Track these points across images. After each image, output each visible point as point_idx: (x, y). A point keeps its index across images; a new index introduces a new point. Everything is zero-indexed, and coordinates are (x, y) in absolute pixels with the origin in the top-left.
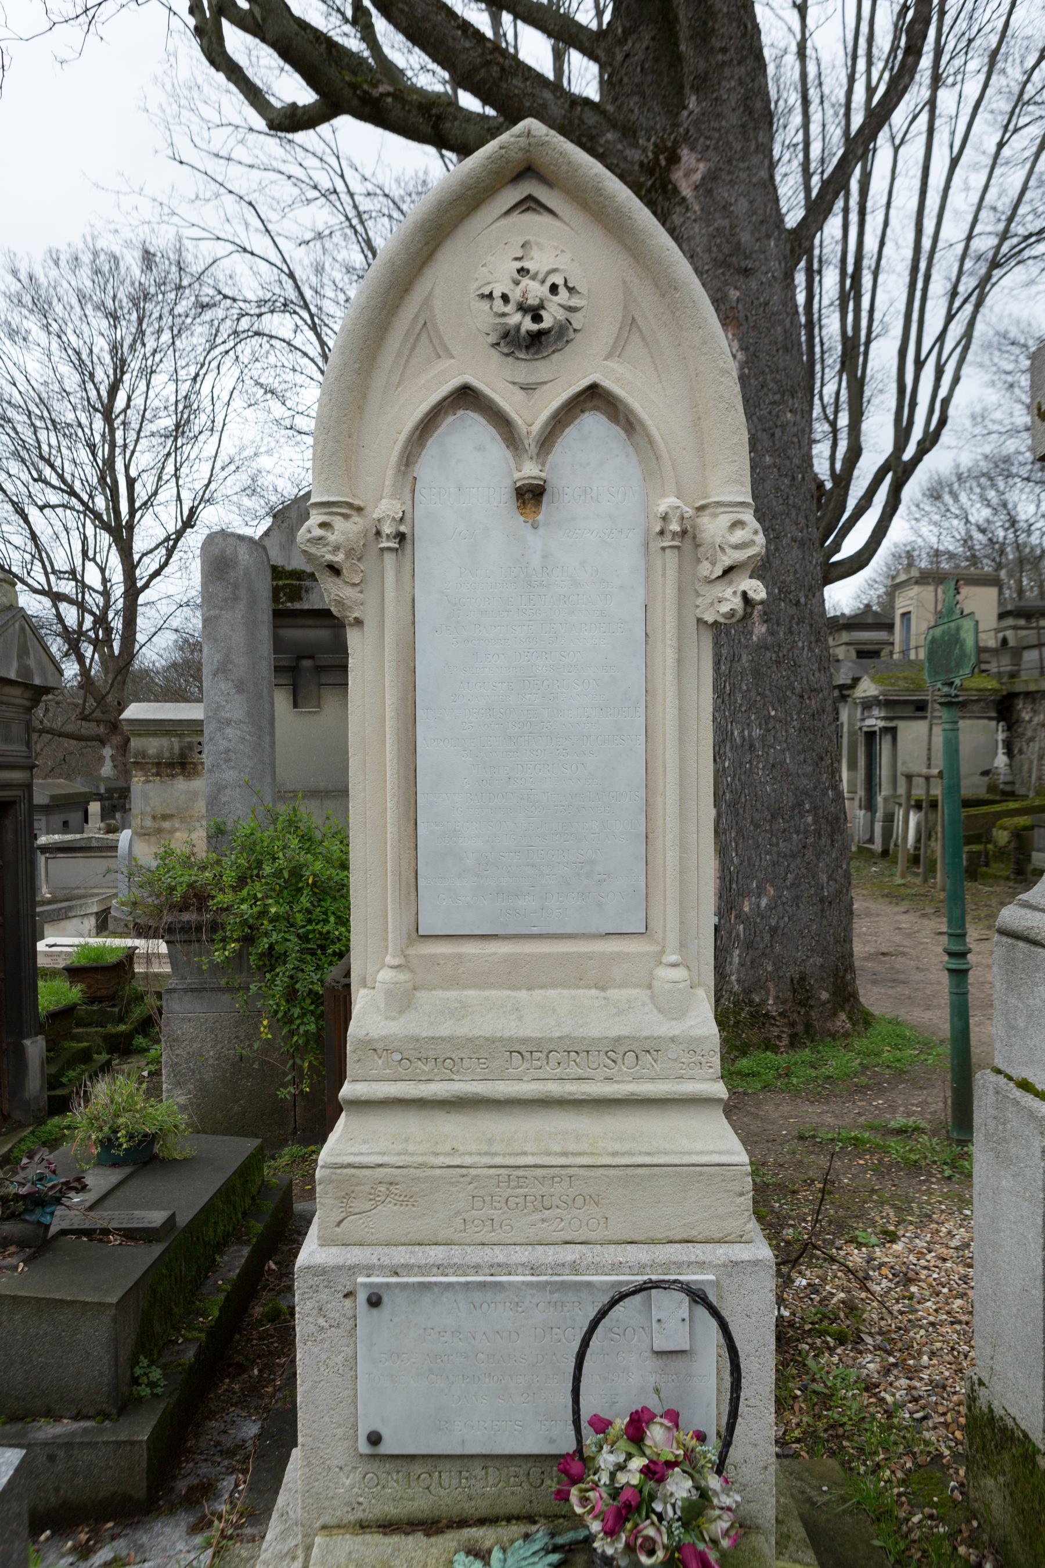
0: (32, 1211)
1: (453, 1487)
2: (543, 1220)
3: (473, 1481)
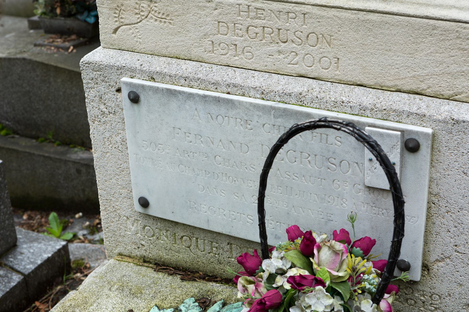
0: (82, 13)
1: (207, 251)
2: (280, 52)
3: (221, 251)
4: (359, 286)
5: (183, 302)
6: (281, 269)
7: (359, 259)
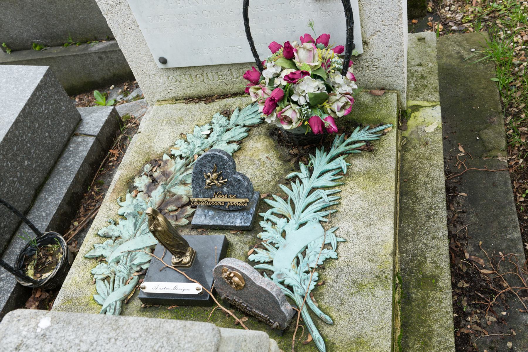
1: (216, 80)
3: (225, 77)
4: (331, 67)
5: (213, 118)
6: (276, 74)
7: (324, 50)
